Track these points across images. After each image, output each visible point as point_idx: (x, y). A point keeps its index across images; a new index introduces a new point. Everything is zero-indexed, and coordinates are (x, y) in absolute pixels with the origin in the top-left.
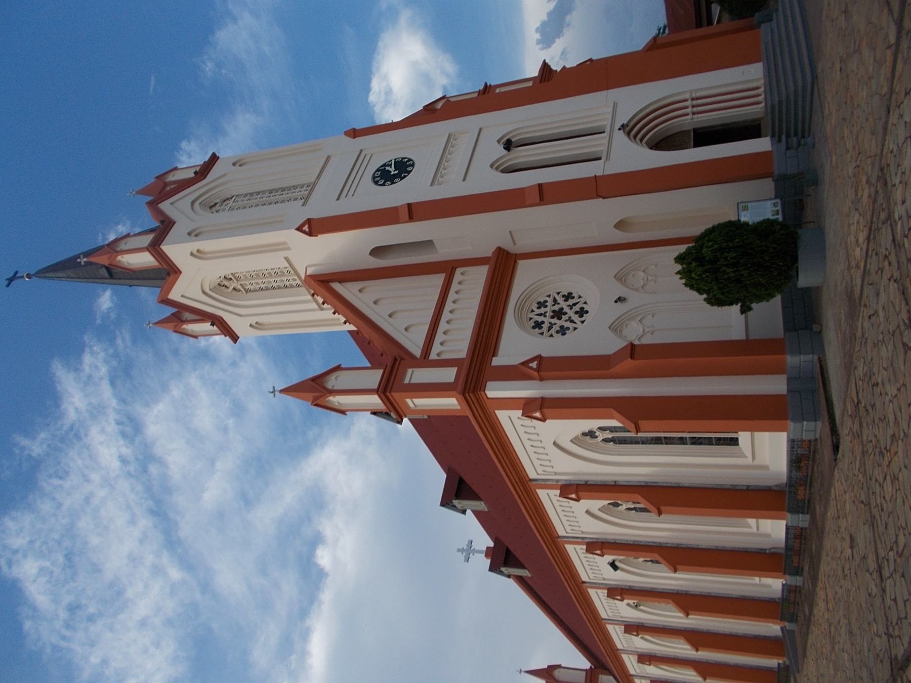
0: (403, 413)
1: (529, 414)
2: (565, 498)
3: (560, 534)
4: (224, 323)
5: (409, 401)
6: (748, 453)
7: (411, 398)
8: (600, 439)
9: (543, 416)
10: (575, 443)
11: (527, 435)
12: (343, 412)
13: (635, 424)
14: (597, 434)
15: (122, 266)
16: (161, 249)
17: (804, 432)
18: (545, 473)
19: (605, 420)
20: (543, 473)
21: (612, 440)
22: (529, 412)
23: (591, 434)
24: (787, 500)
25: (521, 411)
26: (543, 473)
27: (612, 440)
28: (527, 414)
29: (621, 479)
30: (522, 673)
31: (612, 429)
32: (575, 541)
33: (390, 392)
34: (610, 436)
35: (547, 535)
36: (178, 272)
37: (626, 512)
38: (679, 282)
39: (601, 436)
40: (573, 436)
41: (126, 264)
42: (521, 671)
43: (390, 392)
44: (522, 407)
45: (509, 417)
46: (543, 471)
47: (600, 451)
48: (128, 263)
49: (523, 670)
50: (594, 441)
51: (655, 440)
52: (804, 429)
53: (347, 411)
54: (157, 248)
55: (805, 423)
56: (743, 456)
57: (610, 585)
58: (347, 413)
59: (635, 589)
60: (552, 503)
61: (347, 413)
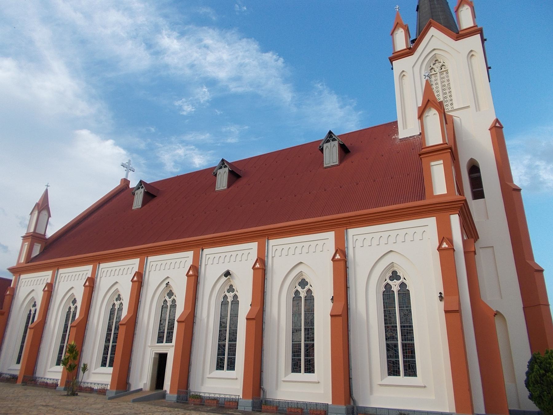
0: (25, 239)
1: (88, 280)
2: (87, 279)
3: (101, 265)
4: (462, 38)
5: (27, 243)
6: (212, 375)
7: (28, 244)
8: (116, 302)
9: (133, 281)
10: (71, 294)
11: (119, 270)
12: (31, 214)
13: (184, 321)
14: (34, 307)
15: (396, 30)
16: (478, 34)
17: (244, 407)
18: (61, 278)
19: (79, 311)
20: (22, 281)
21: (30, 314)
22: (89, 280)
23: (34, 305)
24: (183, 390)
25: (90, 276)
26: (22, 281)
27: (30, 314)
28: (88, 279)
29: (50, 312)
30: (46, 187)
31: (120, 309)
32: (54, 277)
33: (31, 238)
34: (32, 313)
35: (35, 268)
36: (457, 39)
37: (68, 307)
38: (527, 366)
39: (117, 303)
40: (75, 294)
41: (396, 32)
42: (48, 186)
43: (31, 238)
44: (139, 271)
45: (188, 257)
46: (62, 277)
47: (218, 295)
48: (397, 33)
49: (48, 188)
50: (31, 306)
51: (110, 329)
52: (245, 407)
53: (31, 216)
54: (480, 32)
55: (251, 408)
56: (210, 372)
57: (17, 290)
58: (30, 215)
59: (13, 301)
60: (76, 272)
61: (30, 215)
